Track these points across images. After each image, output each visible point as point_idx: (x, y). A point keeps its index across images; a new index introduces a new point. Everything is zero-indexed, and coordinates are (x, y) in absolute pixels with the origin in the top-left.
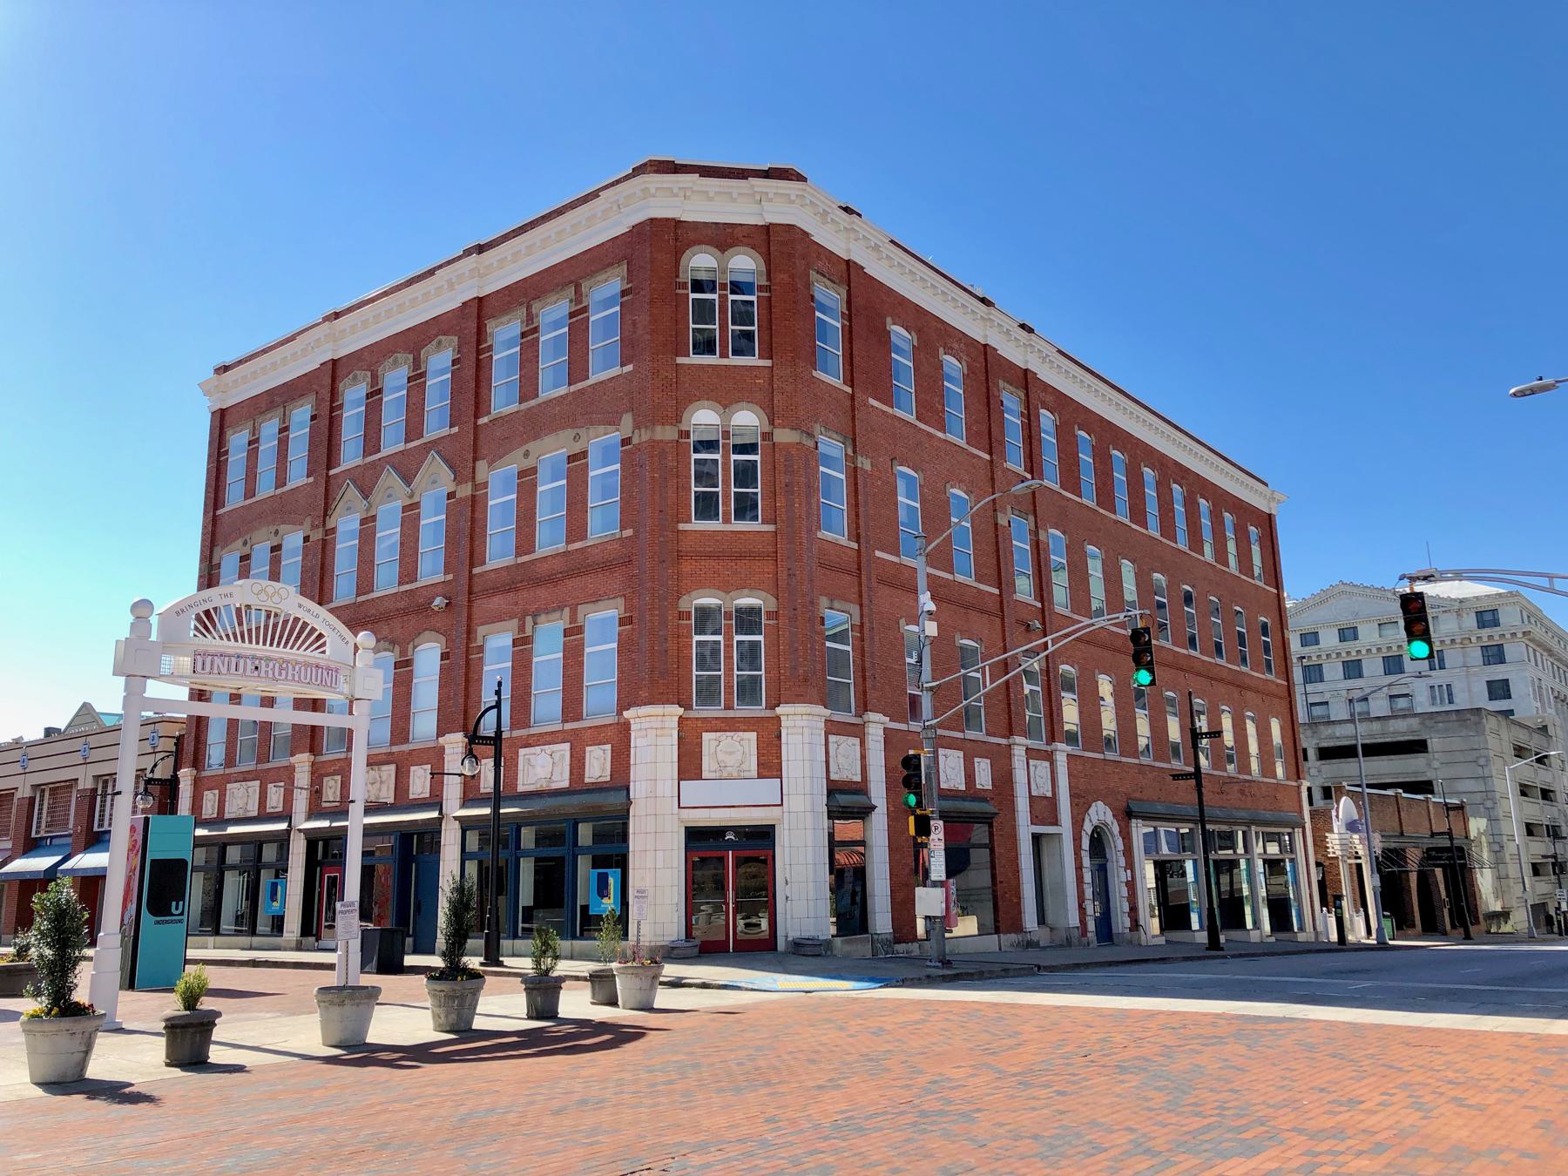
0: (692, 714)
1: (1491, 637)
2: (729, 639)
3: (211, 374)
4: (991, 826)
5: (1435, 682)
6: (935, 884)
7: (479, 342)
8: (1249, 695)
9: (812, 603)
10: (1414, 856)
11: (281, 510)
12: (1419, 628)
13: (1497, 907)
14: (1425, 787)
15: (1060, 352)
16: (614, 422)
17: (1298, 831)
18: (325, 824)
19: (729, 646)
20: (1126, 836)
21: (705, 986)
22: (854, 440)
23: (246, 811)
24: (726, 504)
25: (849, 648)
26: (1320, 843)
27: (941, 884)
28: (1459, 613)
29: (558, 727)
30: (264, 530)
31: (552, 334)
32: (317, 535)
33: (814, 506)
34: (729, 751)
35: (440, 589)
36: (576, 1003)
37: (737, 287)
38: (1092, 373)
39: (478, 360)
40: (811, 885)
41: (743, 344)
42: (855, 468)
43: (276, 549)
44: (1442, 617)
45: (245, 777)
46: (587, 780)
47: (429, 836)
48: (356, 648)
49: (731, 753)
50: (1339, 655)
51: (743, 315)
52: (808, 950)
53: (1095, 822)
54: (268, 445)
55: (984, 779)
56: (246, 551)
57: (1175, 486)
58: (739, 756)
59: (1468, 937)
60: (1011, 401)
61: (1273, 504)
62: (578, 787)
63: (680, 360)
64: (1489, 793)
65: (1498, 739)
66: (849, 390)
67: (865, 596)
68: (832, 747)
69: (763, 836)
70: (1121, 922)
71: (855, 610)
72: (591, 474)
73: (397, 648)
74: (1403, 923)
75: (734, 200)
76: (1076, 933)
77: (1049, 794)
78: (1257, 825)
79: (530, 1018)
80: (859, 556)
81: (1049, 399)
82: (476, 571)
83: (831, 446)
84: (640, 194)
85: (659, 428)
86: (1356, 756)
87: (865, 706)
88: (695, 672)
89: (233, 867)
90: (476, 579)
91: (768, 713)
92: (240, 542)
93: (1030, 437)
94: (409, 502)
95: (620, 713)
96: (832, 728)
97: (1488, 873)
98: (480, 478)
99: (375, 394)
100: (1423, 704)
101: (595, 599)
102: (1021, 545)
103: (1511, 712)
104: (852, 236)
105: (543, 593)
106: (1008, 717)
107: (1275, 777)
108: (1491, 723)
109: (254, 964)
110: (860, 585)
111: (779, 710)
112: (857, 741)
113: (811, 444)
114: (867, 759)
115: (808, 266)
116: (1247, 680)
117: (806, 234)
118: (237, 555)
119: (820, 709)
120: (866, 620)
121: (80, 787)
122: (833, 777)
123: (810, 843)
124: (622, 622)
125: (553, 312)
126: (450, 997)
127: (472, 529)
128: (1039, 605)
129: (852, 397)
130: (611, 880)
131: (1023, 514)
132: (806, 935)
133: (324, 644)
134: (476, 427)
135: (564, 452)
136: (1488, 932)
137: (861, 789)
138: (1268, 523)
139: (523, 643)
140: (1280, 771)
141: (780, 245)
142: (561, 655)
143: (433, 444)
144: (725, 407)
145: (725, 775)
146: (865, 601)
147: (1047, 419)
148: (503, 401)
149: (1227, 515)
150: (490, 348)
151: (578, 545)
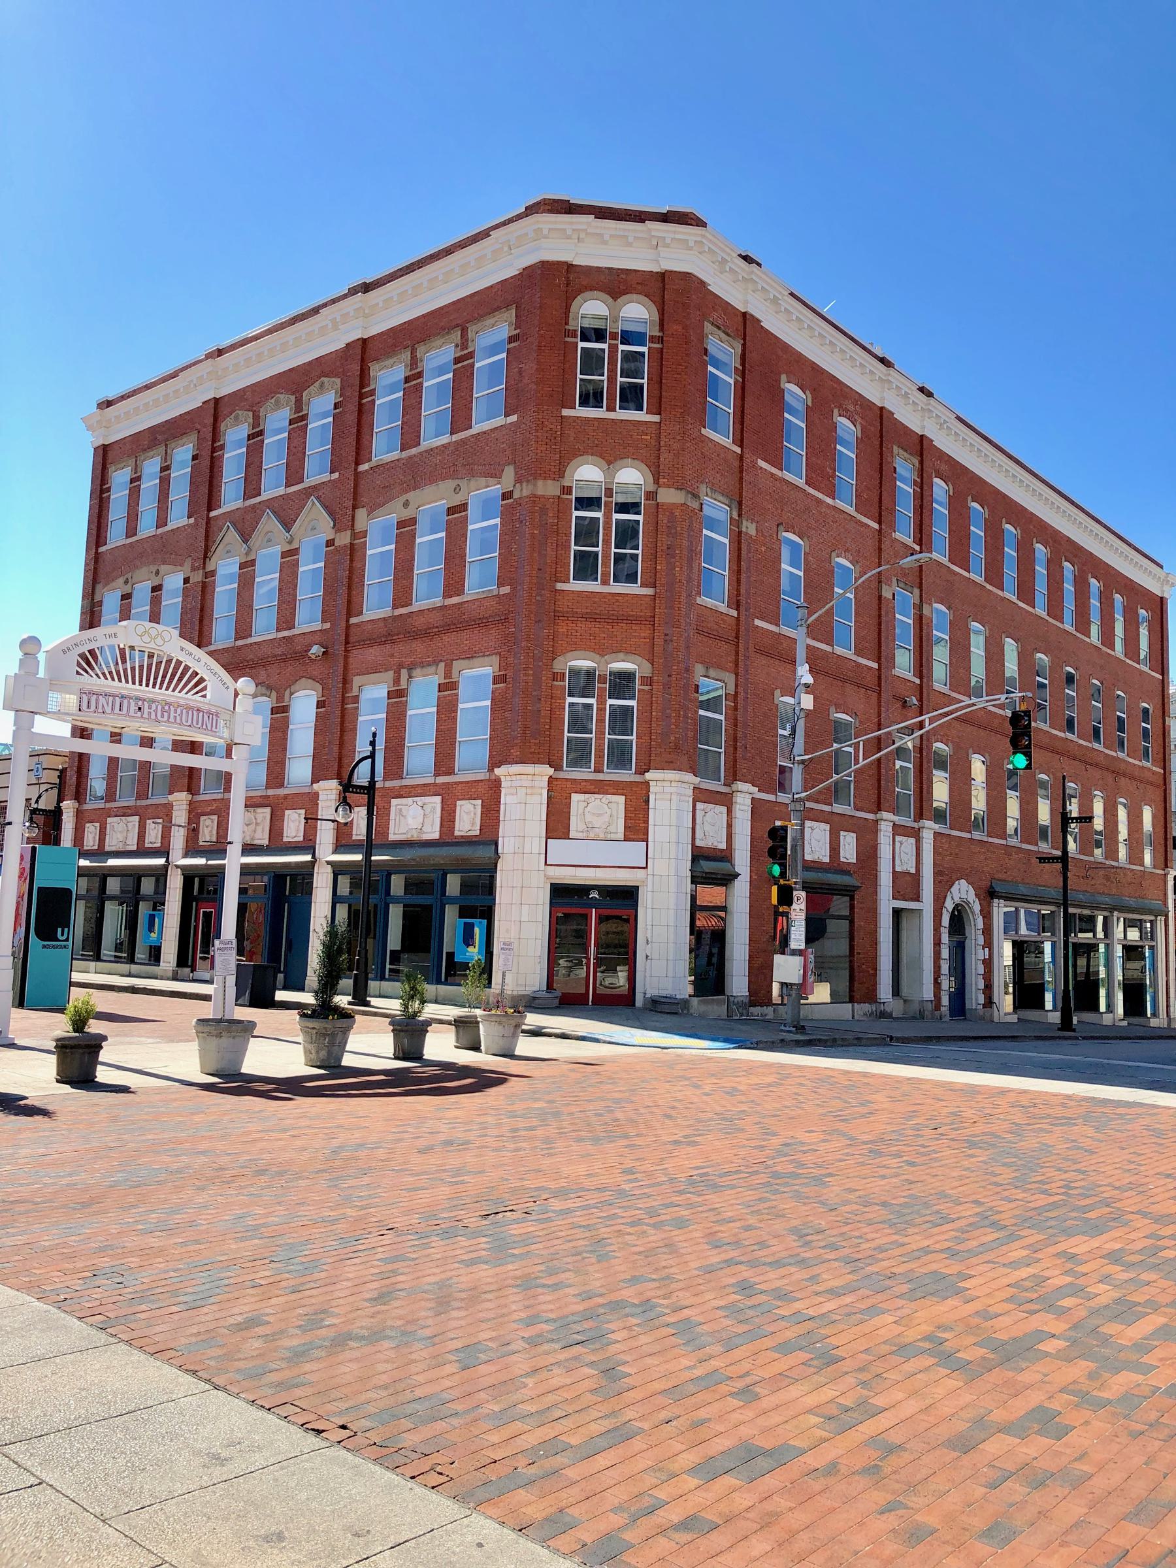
0: (561, 775)
2: (601, 702)
4: (852, 898)
6: (794, 953)
8: (1123, 781)
9: (687, 670)
11: (162, 550)
18: (201, 861)
19: (601, 710)
20: (987, 915)
21: (564, 1036)
22: (740, 504)
24: (606, 564)
27: (799, 953)
30: (144, 570)
32: (197, 577)
33: (695, 570)
36: (440, 1046)
37: (627, 337)
39: (360, 405)
40: (671, 946)
41: (632, 396)
42: (740, 533)
43: (156, 589)
45: (125, 812)
46: (457, 833)
47: (302, 878)
48: (236, 695)
49: (599, 815)
52: (666, 1008)
53: (957, 900)
54: (150, 484)
56: (127, 589)
58: (606, 818)
60: (904, 467)
61: (1166, 588)
62: (448, 839)
63: (566, 412)
66: (738, 450)
67: (741, 664)
69: (627, 896)
70: (975, 998)
71: (730, 678)
73: (274, 694)
75: (630, 245)
76: (930, 1007)
77: (913, 871)
79: (396, 1058)
80: (738, 625)
81: (944, 467)
82: (353, 620)
83: (716, 508)
85: (540, 483)
89: (112, 898)
90: (353, 630)
91: (638, 778)
92: (121, 580)
93: (921, 506)
94: (288, 548)
96: (701, 796)
98: (359, 526)
101: (470, 655)
102: (904, 619)
105: (418, 647)
107: (1142, 865)
109: (133, 990)
110: (737, 653)
111: (648, 776)
112: (724, 809)
113: (696, 505)
114: (734, 827)
115: (704, 317)
118: (119, 594)
120: (740, 689)
122: (698, 843)
123: (672, 906)
124: (496, 680)
125: (439, 356)
127: (350, 578)
128: (918, 681)
129: (741, 458)
130: (477, 930)
131: (907, 586)
132: (663, 993)
133: (205, 688)
135: (444, 504)
137: (725, 856)
139: (397, 696)
140: (1148, 859)
141: (674, 293)
142: (435, 709)
144: (609, 463)
145: (592, 836)
146: (741, 670)
147: (940, 488)
148: (384, 448)
149: (1117, 596)
151: (455, 600)
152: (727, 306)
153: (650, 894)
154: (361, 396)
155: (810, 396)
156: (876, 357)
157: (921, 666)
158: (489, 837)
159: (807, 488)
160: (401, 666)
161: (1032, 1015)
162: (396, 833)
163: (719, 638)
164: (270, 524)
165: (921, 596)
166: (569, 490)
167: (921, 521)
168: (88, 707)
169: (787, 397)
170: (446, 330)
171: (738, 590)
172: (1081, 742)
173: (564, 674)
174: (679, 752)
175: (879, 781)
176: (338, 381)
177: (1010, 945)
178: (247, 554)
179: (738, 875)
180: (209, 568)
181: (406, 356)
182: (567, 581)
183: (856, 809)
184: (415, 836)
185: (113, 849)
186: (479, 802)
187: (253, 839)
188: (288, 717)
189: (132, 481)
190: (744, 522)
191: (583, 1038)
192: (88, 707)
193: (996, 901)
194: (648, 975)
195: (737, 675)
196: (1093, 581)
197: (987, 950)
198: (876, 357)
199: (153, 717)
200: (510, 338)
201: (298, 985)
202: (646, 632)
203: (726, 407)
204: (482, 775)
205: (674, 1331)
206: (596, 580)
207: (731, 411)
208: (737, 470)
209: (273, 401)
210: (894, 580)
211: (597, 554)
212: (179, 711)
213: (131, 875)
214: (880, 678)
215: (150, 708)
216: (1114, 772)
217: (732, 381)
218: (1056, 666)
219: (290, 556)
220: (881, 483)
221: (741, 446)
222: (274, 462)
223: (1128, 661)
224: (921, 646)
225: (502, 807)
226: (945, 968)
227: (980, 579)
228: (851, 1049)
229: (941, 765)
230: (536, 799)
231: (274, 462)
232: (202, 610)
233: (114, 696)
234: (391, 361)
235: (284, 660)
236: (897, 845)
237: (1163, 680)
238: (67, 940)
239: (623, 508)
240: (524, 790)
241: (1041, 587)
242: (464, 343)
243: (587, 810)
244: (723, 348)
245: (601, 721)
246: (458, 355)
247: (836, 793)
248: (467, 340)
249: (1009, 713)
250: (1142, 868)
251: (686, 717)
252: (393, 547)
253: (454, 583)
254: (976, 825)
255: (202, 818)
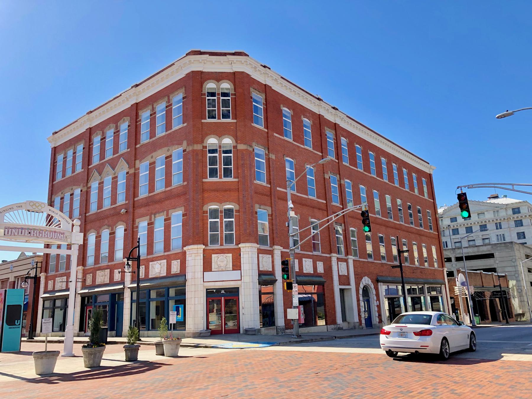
0: (208, 248)
1: (517, 217)
2: (221, 220)
4: (323, 286)
5: (499, 234)
6: (295, 307)
7: (136, 119)
8: (424, 238)
9: (252, 206)
10: (488, 294)
11: (74, 181)
12: (465, 206)
13: (521, 312)
14: (494, 270)
16: (180, 144)
17: (443, 286)
18: (86, 291)
19: (221, 223)
20: (377, 289)
21: (206, 347)
22: (268, 148)
23: (62, 287)
25: (356, 239)
26: (452, 290)
27: (297, 307)
28: (506, 209)
29: (162, 254)
31: (160, 115)
32: (85, 189)
33: (253, 171)
36: (146, 354)
37: (224, 94)
42: (269, 158)
43: (72, 195)
44: (500, 211)
45: (62, 275)
47: (121, 293)
48: (73, 225)
50: (464, 225)
52: (250, 333)
53: (364, 284)
54: (70, 158)
55: (321, 268)
56: (62, 196)
57: (394, 164)
58: (225, 262)
59: (507, 323)
60: (330, 134)
62: (169, 275)
63: (203, 121)
64: (516, 272)
65: (519, 253)
66: (266, 130)
71: (269, 209)
73: (110, 228)
74: (484, 318)
76: (357, 324)
77: (346, 274)
79: (126, 361)
81: (344, 134)
82: (136, 199)
83: (259, 150)
84: (188, 62)
85: (195, 145)
86: (463, 260)
87: (274, 243)
88: (209, 233)
89: (58, 307)
90: (136, 203)
91: (236, 247)
92: (60, 193)
94: (114, 176)
97: (517, 300)
98: (137, 166)
99: (103, 139)
100: (494, 240)
101: (174, 207)
103: (526, 243)
104: (266, 75)
105: (157, 206)
107: (434, 267)
108: (516, 247)
111: (240, 246)
112: (270, 256)
113: (251, 149)
114: (273, 262)
115: (249, 86)
117: (248, 75)
118: (60, 198)
119: (255, 245)
120: (273, 212)
121: (10, 280)
122: (261, 269)
123: (251, 294)
124: (183, 215)
125: (161, 106)
129: (268, 133)
130: (180, 309)
132: (250, 327)
135: (164, 156)
136: (517, 321)
137: (272, 273)
138: (429, 177)
141: (239, 79)
142: (163, 228)
143: (122, 155)
144: (219, 137)
145: (220, 270)
147: (344, 141)
148: (144, 139)
149: (414, 174)
150: (140, 120)
151: (169, 189)
152: (258, 82)
153: (243, 290)
154: (136, 122)
156: (316, 98)
158: (183, 273)
160: (152, 214)
163: (263, 194)
164: (108, 168)
168: (8, 233)
169: (283, 112)
170: (164, 97)
172: (406, 225)
174: (251, 235)
175: (330, 242)
176: (129, 118)
177: (387, 299)
178: (101, 179)
180: (89, 186)
181: (150, 107)
182: (207, 178)
183: (322, 253)
186: (179, 261)
187: (104, 281)
189: (64, 158)
191: (213, 347)
192: (8, 233)
193: (379, 283)
195: (272, 207)
196: (404, 169)
198: (316, 98)
199: (35, 235)
203: (261, 117)
204: (179, 251)
206: (217, 177)
210: (329, 172)
211: (217, 169)
212: (35, 232)
213: (63, 298)
214: (327, 205)
215: (34, 232)
217: (262, 107)
218: (404, 204)
219: (115, 178)
221: (267, 129)
222: (109, 146)
226: (363, 309)
228: (318, 343)
229: (368, 238)
230: (199, 258)
231: (109, 146)
232: (86, 201)
233: (19, 229)
235: (114, 215)
236: (339, 265)
238: (19, 325)
239: (225, 152)
240: (195, 254)
241: (406, 182)
244: (258, 96)
245: (222, 227)
247: (315, 247)
249: (361, 212)
253: (168, 183)
254: (370, 256)
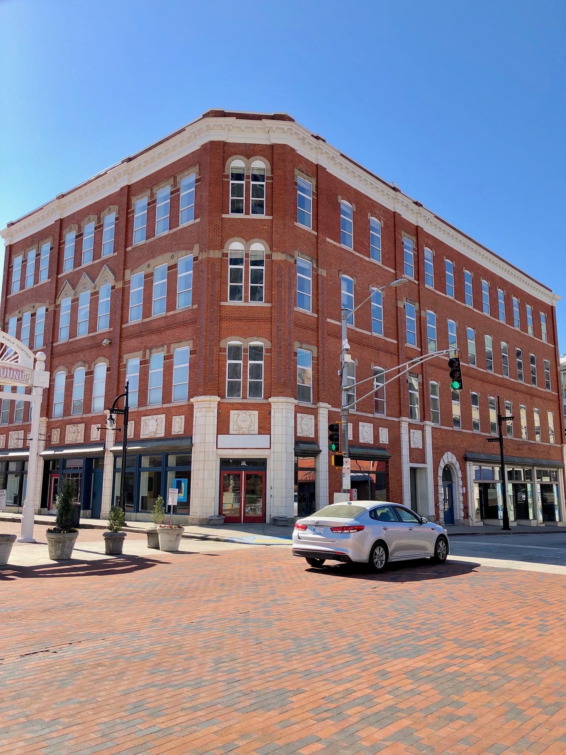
0: (224, 401)
2: (245, 362)
3: (6, 226)
4: (387, 462)
6: (345, 491)
8: (536, 400)
9: (290, 345)
15: (436, 217)
18: (51, 452)
19: (245, 366)
20: (464, 470)
21: (217, 540)
22: (317, 260)
23: (18, 445)
24: (246, 292)
29: (160, 406)
30: (28, 305)
31: (162, 204)
32: (52, 308)
33: (293, 294)
34: (244, 420)
35: (107, 336)
36: (134, 546)
37: (255, 178)
38: (454, 229)
39: (127, 217)
40: (284, 490)
41: (258, 207)
42: (318, 275)
43: (33, 315)
45: (17, 429)
46: (173, 433)
47: (99, 459)
49: (244, 421)
51: (258, 192)
53: (446, 462)
54: (31, 262)
55: (384, 437)
56: (20, 316)
58: (249, 423)
60: (408, 242)
61: (554, 302)
62: (169, 437)
63: (224, 216)
66: (315, 233)
67: (320, 342)
68: (299, 420)
69: (261, 464)
70: (459, 514)
71: (315, 349)
72: (179, 276)
73: (87, 365)
75: (255, 131)
77: (421, 447)
78: (538, 466)
79: (107, 554)
80: (318, 321)
81: (430, 242)
82: (124, 326)
83: (304, 262)
85: (211, 252)
89: (12, 473)
90: (124, 331)
91: (265, 401)
92: (17, 312)
93: (418, 261)
95: (189, 400)
96: (298, 410)
98: (127, 278)
101: (179, 341)
102: (411, 318)
104: (319, 151)
105: (154, 337)
106: (401, 408)
107: (549, 442)
110: (318, 336)
112: (313, 417)
113: (292, 261)
114: (315, 426)
115: (294, 166)
116: (536, 392)
118: (16, 318)
119: (293, 400)
120: (320, 354)
122: (298, 435)
124: (192, 353)
125: (163, 192)
126: (58, 542)
127: (122, 305)
128: (420, 350)
129: (317, 237)
130: (183, 484)
131: (412, 301)
132: (280, 515)
133: (17, 358)
134: (126, 252)
135: (166, 265)
137: (314, 441)
138: (551, 311)
139: (145, 363)
140: (552, 439)
141: (278, 154)
143: (106, 261)
145: (241, 432)
146: (320, 345)
147: (428, 252)
148: (139, 238)
151: (172, 313)
153: (272, 462)
154: (128, 213)
155: (354, 207)
157: (421, 342)
158: (188, 435)
159: (354, 252)
160: (146, 348)
161: (523, 522)
162: (143, 435)
164: (85, 279)
165: (420, 306)
166: (226, 255)
167: (418, 269)
169: (342, 206)
170: (167, 178)
171: (318, 304)
173: (225, 348)
175: (400, 401)
176: (117, 207)
178: (75, 295)
179: (321, 451)
181: (148, 192)
183: (387, 416)
184: (152, 435)
185: (12, 447)
186: (183, 417)
187: (76, 440)
188: (93, 377)
190: (320, 269)
194: (272, 505)
195: (318, 347)
197: (464, 488)
200: (196, 180)
201: (96, 515)
202: (268, 326)
205: (407, 677)
207: (311, 214)
208: (315, 243)
209: (87, 219)
210: (404, 298)
214: (398, 348)
216: (530, 395)
217: (311, 199)
220: (395, 250)
221: (317, 231)
223: (535, 338)
224: (421, 332)
225: (194, 418)
227: (452, 298)
229: (455, 397)
232: (54, 324)
234: (141, 196)
235: (92, 348)
236: (412, 434)
237: (555, 348)
239: (254, 263)
240: (206, 409)
242: (175, 184)
243: (238, 419)
244: (306, 183)
246: (173, 190)
248: (176, 182)
250: (548, 444)
251: (290, 369)
252: (142, 288)
255: (53, 430)
